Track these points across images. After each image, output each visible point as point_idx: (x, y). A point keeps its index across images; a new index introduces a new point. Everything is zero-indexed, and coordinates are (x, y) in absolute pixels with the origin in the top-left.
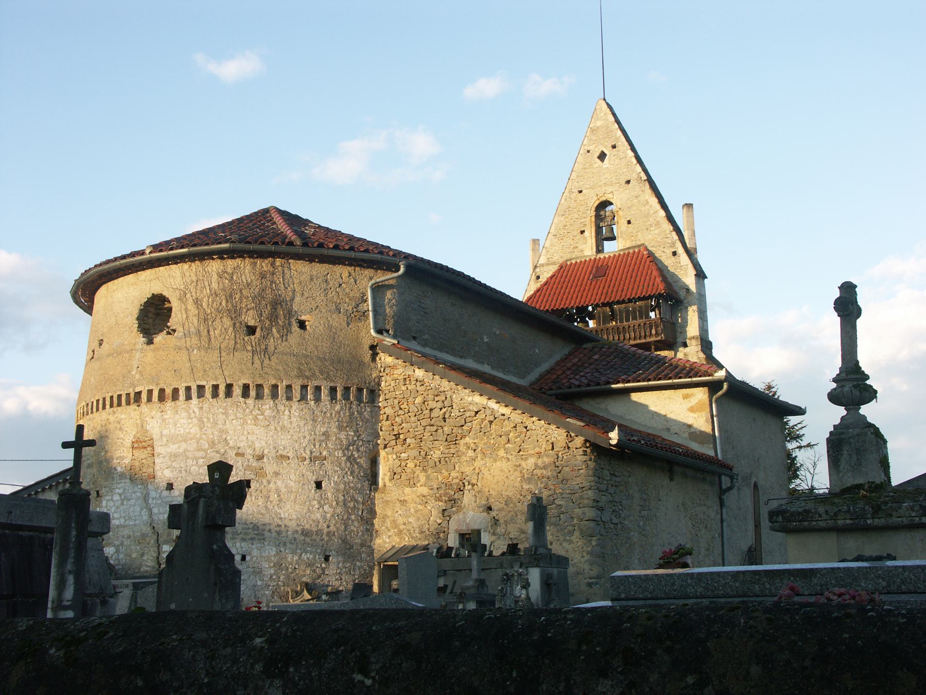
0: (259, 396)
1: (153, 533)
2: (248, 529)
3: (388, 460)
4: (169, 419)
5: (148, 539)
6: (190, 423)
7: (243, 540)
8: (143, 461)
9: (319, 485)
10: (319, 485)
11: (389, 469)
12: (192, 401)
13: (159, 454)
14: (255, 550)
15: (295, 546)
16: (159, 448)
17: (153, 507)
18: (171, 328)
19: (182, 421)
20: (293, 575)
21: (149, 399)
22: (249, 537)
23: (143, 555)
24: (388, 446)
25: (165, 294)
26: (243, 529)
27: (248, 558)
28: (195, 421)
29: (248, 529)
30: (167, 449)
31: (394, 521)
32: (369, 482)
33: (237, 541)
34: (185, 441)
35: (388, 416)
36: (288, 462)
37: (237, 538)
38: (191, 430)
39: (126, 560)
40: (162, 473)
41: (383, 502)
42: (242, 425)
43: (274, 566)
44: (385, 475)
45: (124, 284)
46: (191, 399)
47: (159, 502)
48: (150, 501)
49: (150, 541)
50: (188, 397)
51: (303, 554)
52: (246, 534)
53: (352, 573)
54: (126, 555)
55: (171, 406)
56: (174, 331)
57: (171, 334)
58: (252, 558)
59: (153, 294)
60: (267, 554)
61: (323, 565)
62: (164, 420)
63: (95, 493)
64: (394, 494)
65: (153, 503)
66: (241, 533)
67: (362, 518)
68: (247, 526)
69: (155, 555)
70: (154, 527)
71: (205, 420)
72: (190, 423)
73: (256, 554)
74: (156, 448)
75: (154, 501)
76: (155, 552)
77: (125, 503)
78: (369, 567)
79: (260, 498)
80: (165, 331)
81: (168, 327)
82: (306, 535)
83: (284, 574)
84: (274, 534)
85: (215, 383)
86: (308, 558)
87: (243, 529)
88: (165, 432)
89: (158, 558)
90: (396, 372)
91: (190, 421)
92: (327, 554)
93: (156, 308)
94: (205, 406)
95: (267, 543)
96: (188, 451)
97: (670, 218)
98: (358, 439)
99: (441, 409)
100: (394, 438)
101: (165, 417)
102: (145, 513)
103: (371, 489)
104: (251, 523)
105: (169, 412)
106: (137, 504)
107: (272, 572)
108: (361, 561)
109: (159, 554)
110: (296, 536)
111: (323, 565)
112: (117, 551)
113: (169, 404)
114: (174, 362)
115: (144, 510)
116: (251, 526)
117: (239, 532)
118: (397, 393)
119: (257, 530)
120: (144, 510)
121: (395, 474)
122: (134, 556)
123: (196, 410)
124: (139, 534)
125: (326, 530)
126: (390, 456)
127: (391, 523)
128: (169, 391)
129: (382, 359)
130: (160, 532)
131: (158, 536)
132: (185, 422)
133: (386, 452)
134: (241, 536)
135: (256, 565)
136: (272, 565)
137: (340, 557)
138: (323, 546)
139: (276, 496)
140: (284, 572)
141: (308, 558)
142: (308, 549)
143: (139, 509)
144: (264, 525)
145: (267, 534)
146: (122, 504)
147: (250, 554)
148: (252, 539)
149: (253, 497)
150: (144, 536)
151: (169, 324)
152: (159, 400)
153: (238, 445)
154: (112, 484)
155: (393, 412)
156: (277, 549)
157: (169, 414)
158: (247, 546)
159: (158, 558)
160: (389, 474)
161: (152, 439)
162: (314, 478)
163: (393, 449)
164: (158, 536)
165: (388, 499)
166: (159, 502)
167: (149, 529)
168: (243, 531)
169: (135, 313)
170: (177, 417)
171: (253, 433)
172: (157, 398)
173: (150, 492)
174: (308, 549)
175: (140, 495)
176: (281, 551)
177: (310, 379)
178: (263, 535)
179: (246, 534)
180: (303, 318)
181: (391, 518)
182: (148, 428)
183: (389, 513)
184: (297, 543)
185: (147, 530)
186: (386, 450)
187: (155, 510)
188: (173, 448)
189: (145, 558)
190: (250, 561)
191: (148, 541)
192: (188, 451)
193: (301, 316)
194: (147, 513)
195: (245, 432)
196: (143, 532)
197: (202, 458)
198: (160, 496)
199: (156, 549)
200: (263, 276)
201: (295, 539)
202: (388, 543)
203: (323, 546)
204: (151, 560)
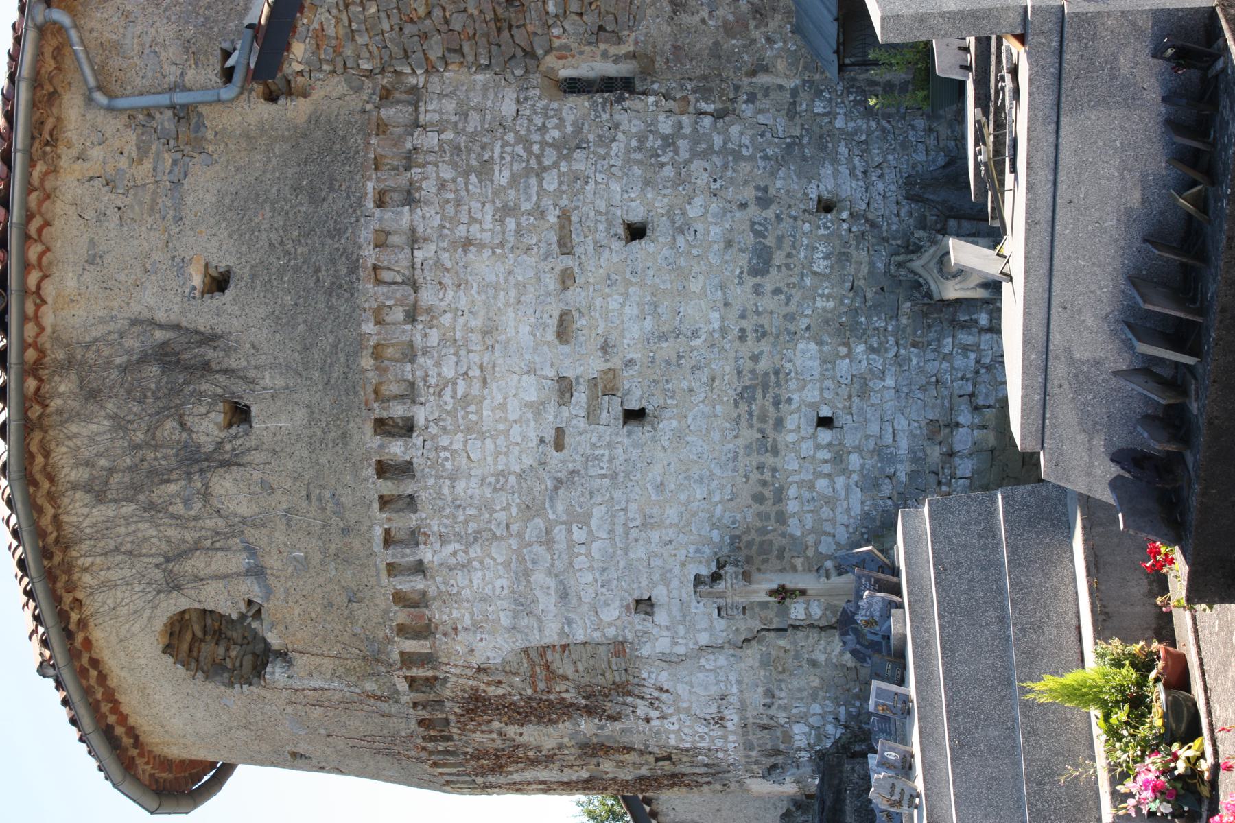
0: (407, 428)
1: (760, 642)
2: (750, 413)
3: (566, 47)
4: (472, 614)
5: (774, 653)
6: (481, 563)
7: (779, 423)
8: (581, 669)
9: (636, 232)
10: (636, 232)
11: (590, 44)
12: (426, 561)
13: (562, 633)
14: (804, 393)
15: (794, 291)
16: (547, 632)
17: (696, 643)
18: (244, 610)
19: (477, 581)
20: (869, 295)
21: (427, 659)
22: (771, 409)
23: (814, 663)
24: (528, 49)
25: (159, 623)
26: (751, 426)
27: (825, 412)
28: (476, 551)
29: (750, 413)
30: (550, 616)
31: (728, 30)
32: (624, 99)
33: (780, 439)
34: (527, 574)
35: (450, 50)
36: (576, 315)
37: (774, 440)
38: (500, 560)
39: (825, 698)
40: (609, 625)
41: (678, 60)
42: (482, 436)
43: (847, 344)
44: (605, 55)
45: (147, 712)
46: (420, 562)
47: (681, 630)
48: (681, 650)
49: (781, 647)
50: (419, 568)
51: (815, 268)
52: (763, 418)
53: (863, 138)
54: (814, 697)
55: (439, 609)
56: (250, 603)
57: (259, 611)
58: (824, 401)
59: (164, 652)
60: (817, 363)
61: (845, 215)
62: (476, 626)
63: (660, 763)
64: (653, 31)
65: (686, 645)
66: (760, 431)
67: (719, 115)
68: (745, 417)
69: (815, 635)
70: (746, 640)
71: (472, 526)
72: (481, 563)
73: (817, 393)
74: (547, 641)
75: (680, 641)
76: (807, 637)
77: (685, 705)
78: (849, 93)
79: (669, 386)
80: (254, 625)
81: (243, 617)
82: (767, 263)
83: (869, 318)
84: (765, 346)
85: (376, 506)
86: (826, 257)
87: (751, 426)
88: (505, 620)
89: (822, 629)
90: (331, 31)
91: (475, 564)
92: (813, 205)
93: (202, 640)
94: (435, 529)
95: (789, 365)
96: (553, 565)
97: (1203, 675)
98: (512, 130)
99: (675, 555)
100: (505, 34)
101: (467, 621)
102: (708, 662)
103: (644, 93)
104: (736, 404)
105: (455, 614)
106: (687, 679)
107: (861, 348)
108: (832, 115)
109: (812, 626)
110: (769, 288)
111: (845, 215)
112: (803, 718)
113: (438, 614)
114: (331, 605)
115: (703, 661)
116: (743, 407)
117: (759, 436)
118: (386, 26)
119: (754, 392)
120: (703, 661)
121: (601, 28)
122: (816, 682)
123: (449, 549)
124: (762, 673)
125: (753, 210)
126: (557, 43)
127: (734, 38)
128: (401, 616)
129: (299, 68)
130: (756, 625)
131: (768, 630)
132: (479, 574)
133: (547, 53)
134: (769, 432)
135: (844, 391)
136: (843, 350)
137: (823, 171)
138: (795, 218)
139: (664, 345)
140: (863, 319)
141: (826, 257)
142: (802, 255)
143: (701, 675)
144: (739, 373)
145: (763, 365)
146: (687, 710)
147: (815, 406)
148: (777, 403)
149: (669, 402)
150: (765, 663)
151: (234, 617)
152: (426, 638)
153: (534, 444)
154: (638, 732)
155: (437, 38)
156: (802, 337)
157: (461, 615)
158: (796, 416)
159: (822, 629)
160: (603, 46)
161: (526, 651)
162: (616, 245)
163: (535, 34)
164: (768, 630)
165: (668, 47)
166: (681, 630)
167: (749, 652)
168: (757, 425)
169: (214, 689)
170: (466, 593)
171: (503, 406)
172: (422, 642)
173: (658, 650)
174: (802, 255)
175: (665, 673)
176: (808, 328)
177: (358, 260)
178: (766, 374)
179: (763, 418)
180: (197, 280)
181: (719, 39)
182: (498, 660)
183: (706, 42)
184: (788, 285)
185: (752, 654)
186: (540, 52)
187: (704, 639)
188: (547, 603)
189: (822, 658)
190: (833, 406)
191: (782, 654)
192: (553, 565)
193: (194, 288)
194: (711, 657)
195: (501, 427)
196: (757, 665)
197: (570, 531)
198: (668, 628)
199: (800, 634)
200: (93, 395)
201: (777, 291)
202: (785, 42)
203: (795, 218)
204: (828, 643)
